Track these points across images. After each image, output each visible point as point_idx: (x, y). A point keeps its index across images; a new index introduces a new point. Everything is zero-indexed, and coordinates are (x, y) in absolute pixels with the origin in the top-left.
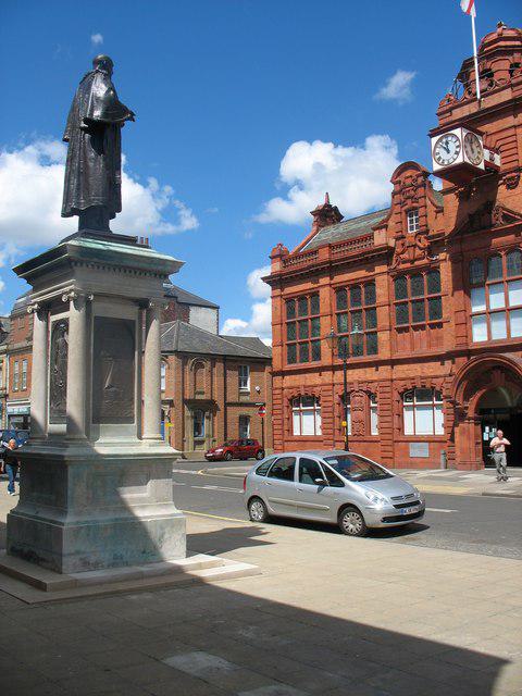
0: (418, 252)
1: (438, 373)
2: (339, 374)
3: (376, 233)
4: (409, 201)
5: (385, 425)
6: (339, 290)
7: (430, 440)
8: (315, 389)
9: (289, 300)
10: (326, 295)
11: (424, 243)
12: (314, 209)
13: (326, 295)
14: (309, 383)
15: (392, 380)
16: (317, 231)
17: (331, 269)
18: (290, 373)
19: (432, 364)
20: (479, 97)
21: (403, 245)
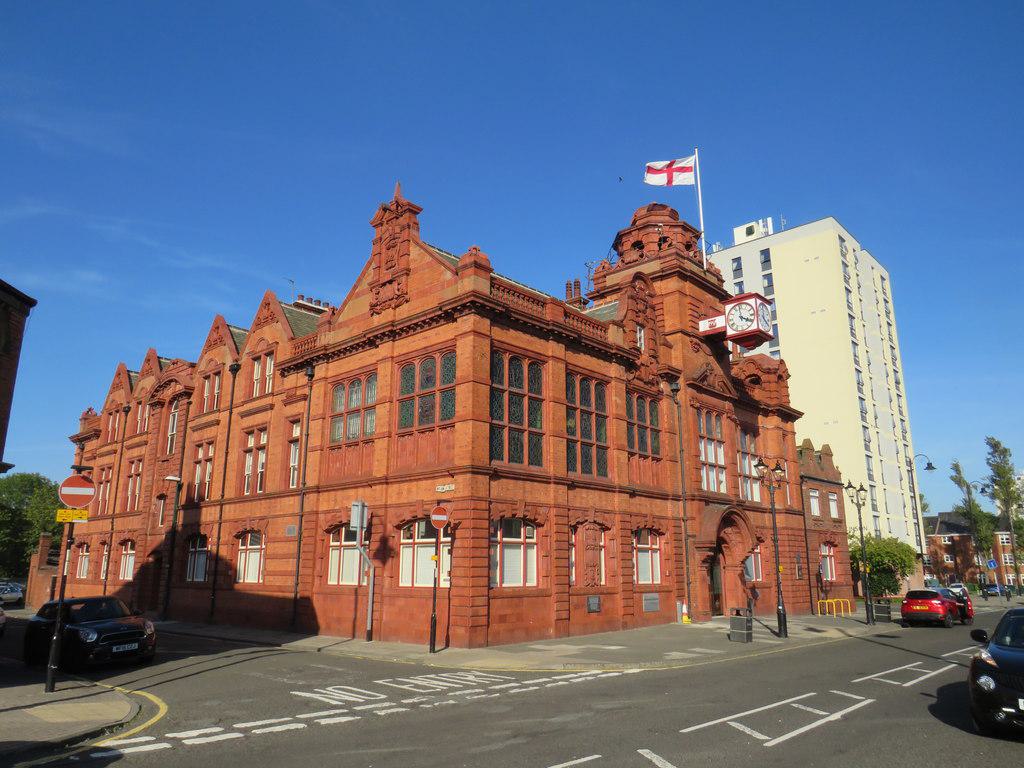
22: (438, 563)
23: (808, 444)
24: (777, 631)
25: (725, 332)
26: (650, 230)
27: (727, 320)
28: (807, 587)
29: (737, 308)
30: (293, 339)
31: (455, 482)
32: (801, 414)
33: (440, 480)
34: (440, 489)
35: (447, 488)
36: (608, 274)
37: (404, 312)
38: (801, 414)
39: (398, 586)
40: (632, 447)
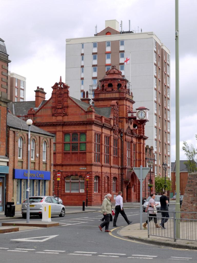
12: (147, 123)
22: (182, 183)
23: (147, 146)
24: (120, 215)
25: (136, 118)
26: (115, 81)
27: (137, 115)
28: (145, 194)
29: (141, 111)
30: (74, 139)
31: (86, 167)
32: (148, 138)
33: (81, 166)
34: (81, 168)
35: (83, 168)
36: (100, 93)
37: (66, 119)
38: (148, 138)
39: (65, 192)
40: (105, 153)
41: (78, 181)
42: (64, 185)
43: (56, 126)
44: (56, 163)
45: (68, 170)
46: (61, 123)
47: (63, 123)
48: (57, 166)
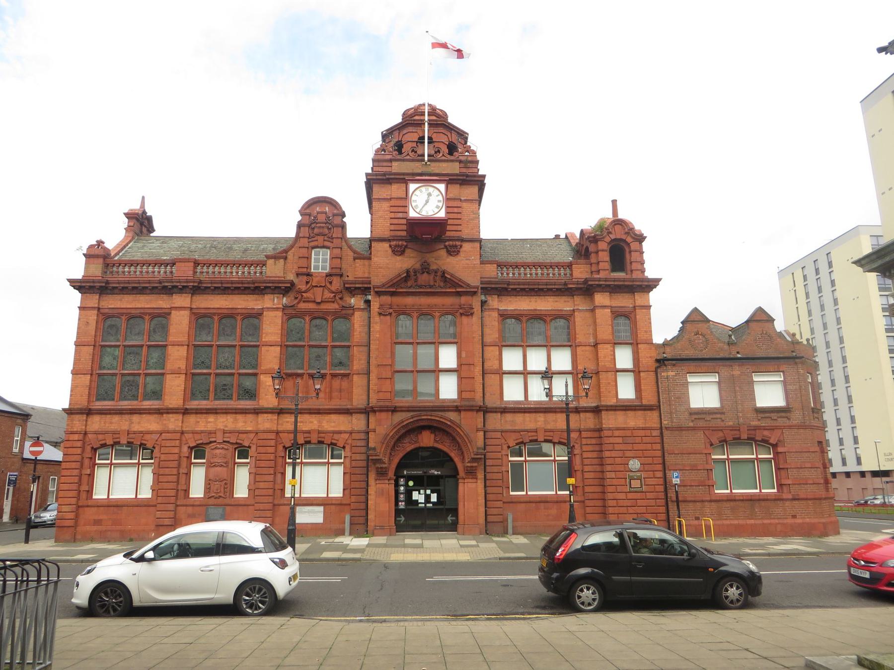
0: (328, 295)
1: (342, 428)
2: (290, 419)
3: (270, 262)
4: (320, 239)
5: (354, 485)
6: (200, 318)
7: (325, 503)
8: (147, 437)
9: (105, 316)
10: (180, 323)
11: (337, 284)
12: (126, 212)
13: (180, 323)
14: (136, 428)
15: (182, 433)
16: (133, 238)
17: (197, 289)
18: (102, 412)
19: (333, 417)
20: (426, 158)
21: (307, 283)
32: (659, 280)
41: (109, 462)
42: (282, 473)
43: (264, 294)
44: (352, 405)
45: (201, 427)
46: (96, 285)
47: (196, 284)
48: (168, 413)
